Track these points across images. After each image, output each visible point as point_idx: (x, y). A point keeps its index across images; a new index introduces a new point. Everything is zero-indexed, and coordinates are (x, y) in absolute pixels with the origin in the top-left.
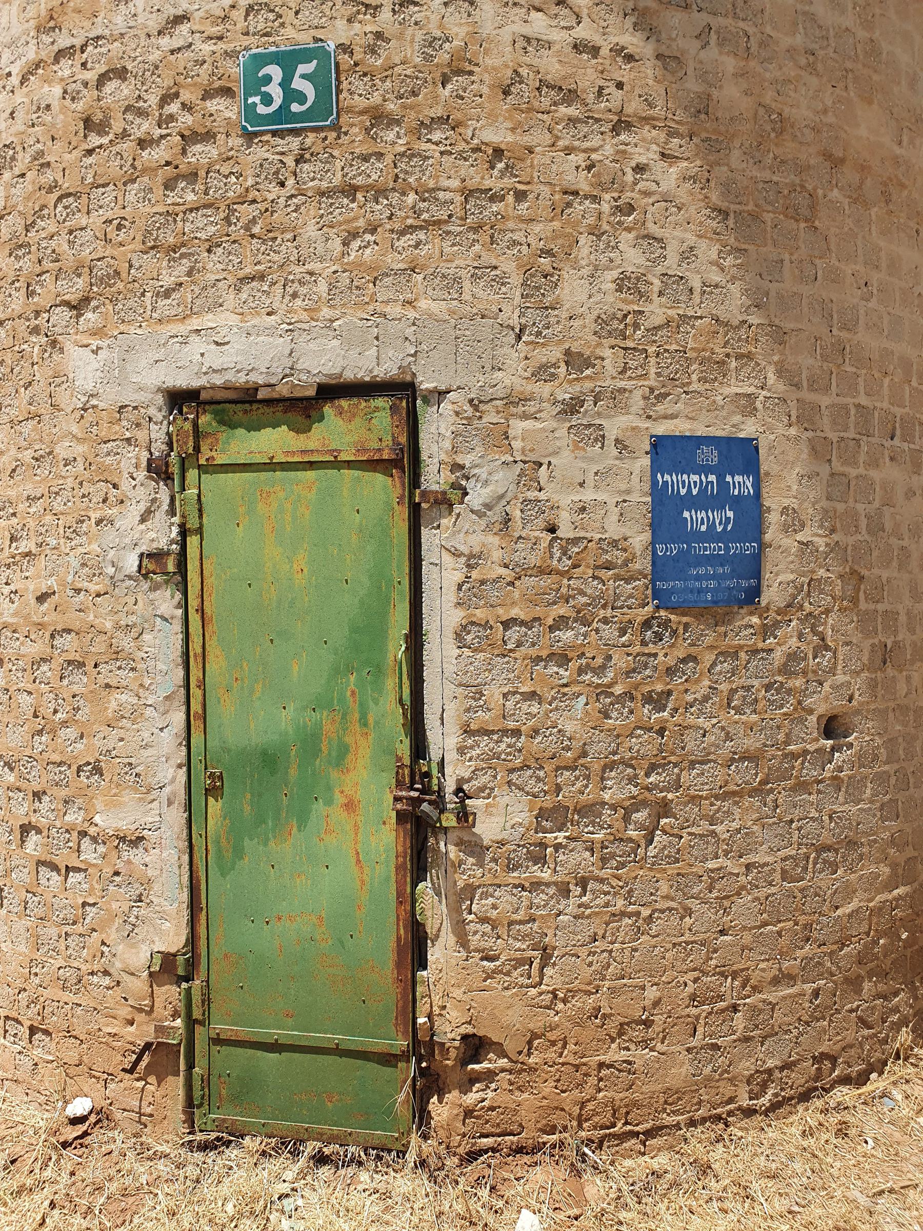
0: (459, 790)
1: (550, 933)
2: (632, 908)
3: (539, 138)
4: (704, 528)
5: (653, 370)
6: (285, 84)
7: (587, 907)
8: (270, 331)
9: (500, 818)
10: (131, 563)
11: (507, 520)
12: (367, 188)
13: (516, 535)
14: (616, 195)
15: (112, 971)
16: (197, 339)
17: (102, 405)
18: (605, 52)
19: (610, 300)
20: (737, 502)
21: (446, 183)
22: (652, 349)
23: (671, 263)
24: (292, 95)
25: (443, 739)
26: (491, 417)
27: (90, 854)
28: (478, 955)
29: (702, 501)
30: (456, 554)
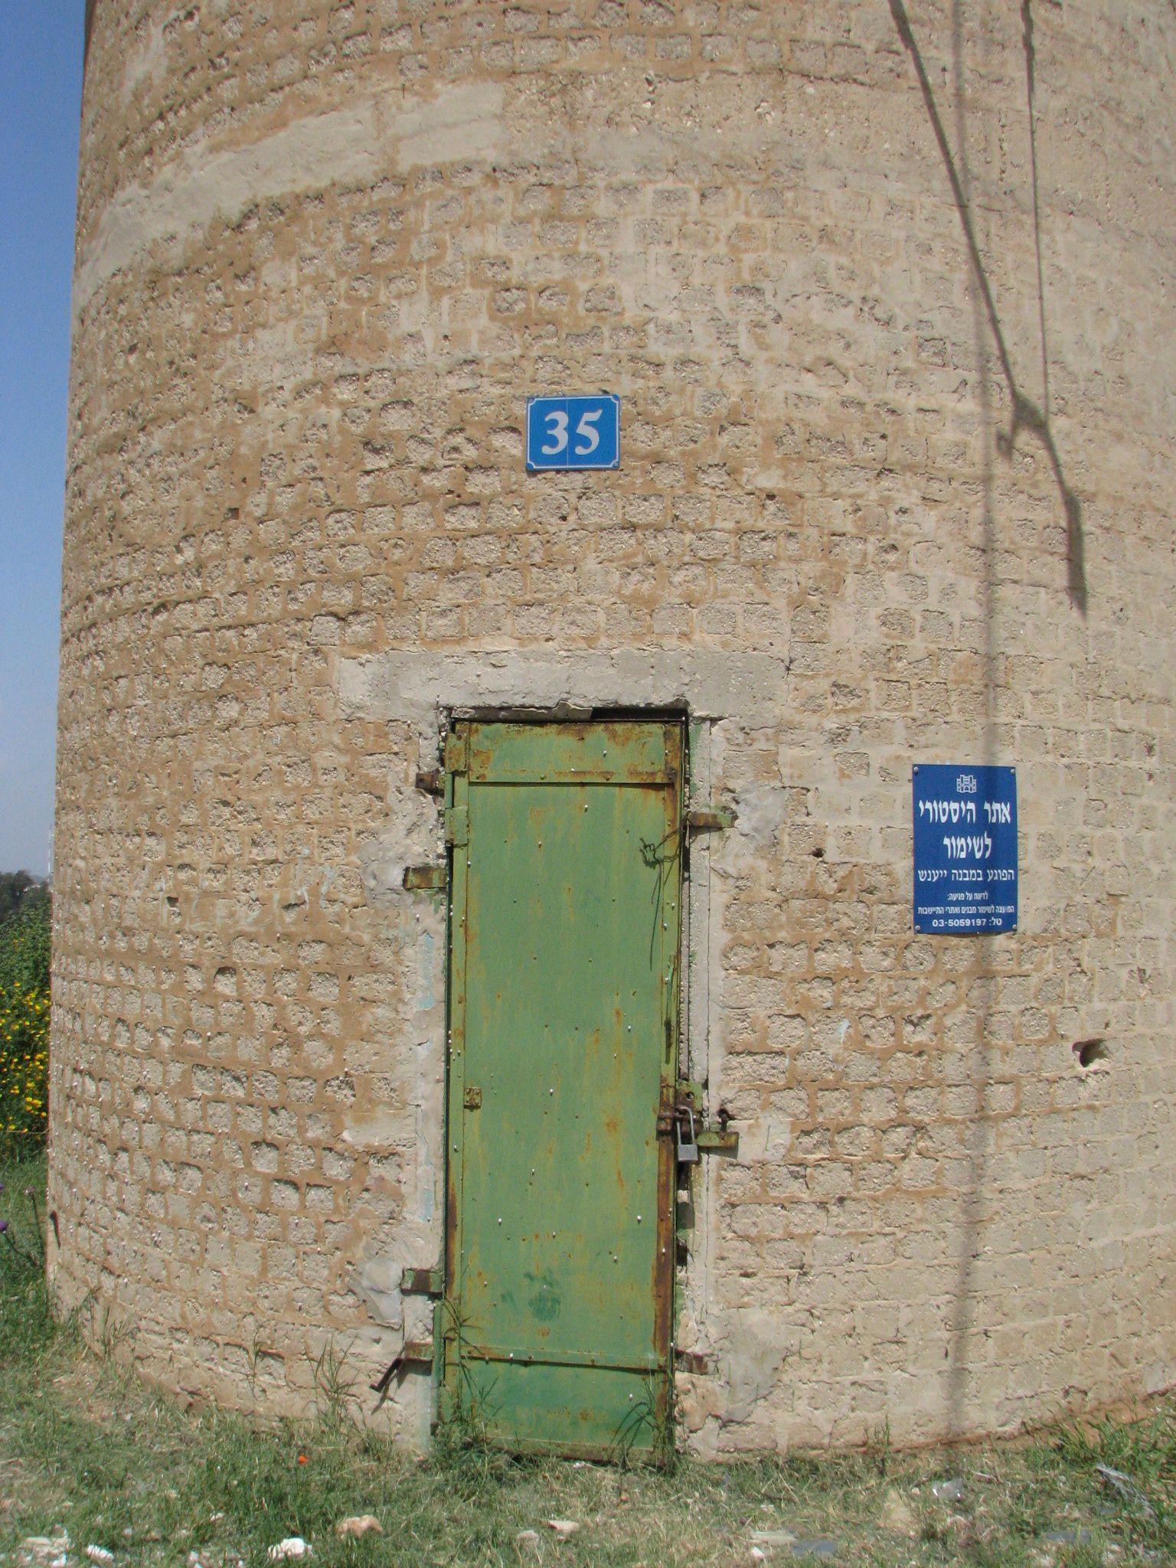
0: (722, 1112)
1: (808, 1251)
2: (887, 1230)
3: (806, 484)
4: (963, 855)
5: (915, 702)
6: (571, 429)
7: (843, 1226)
8: (548, 657)
9: (764, 1137)
10: (396, 876)
11: (775, 842)
12: (647, 526)
13: (784, 858)
14: (880, 537)
15: (357, 1290)
16: (474, 660)
17: (369, 718)
18: (869, 408)
19: (874, 636)
20: (993, 830)
21: (719, 524)
22: (914, 682)
23: (932, 602)
24: (576, 439)
25: (707, 1059)
26: (762, 744)
27: (336, 1169)
28: (737, 1272)
29: (961, 829)
30: (725, 876)
